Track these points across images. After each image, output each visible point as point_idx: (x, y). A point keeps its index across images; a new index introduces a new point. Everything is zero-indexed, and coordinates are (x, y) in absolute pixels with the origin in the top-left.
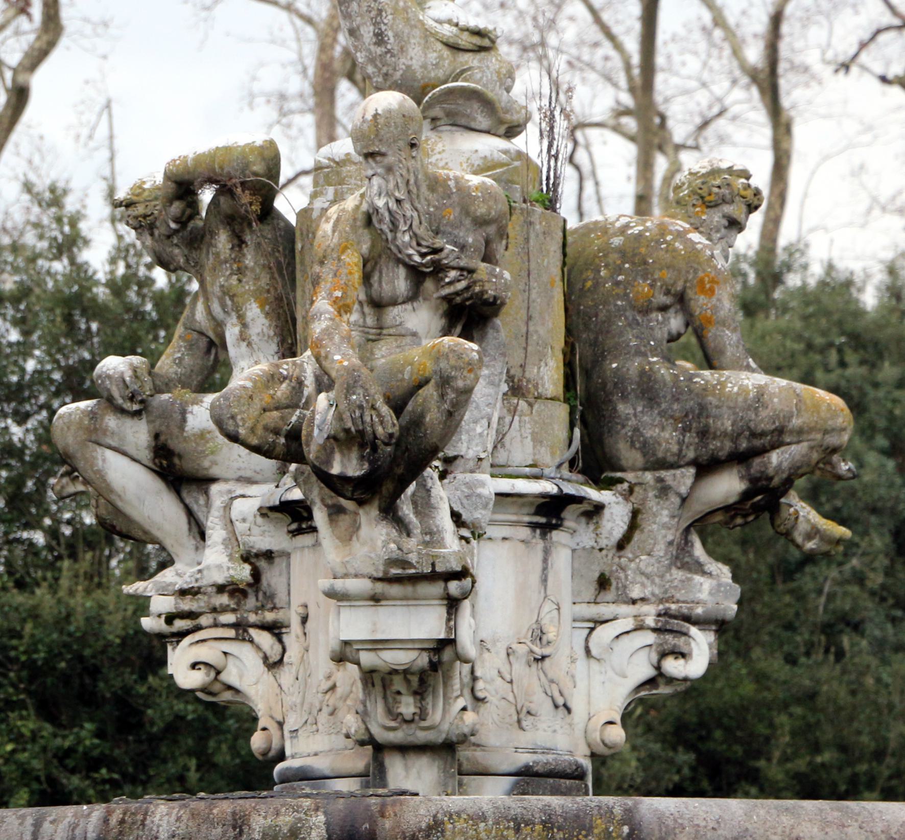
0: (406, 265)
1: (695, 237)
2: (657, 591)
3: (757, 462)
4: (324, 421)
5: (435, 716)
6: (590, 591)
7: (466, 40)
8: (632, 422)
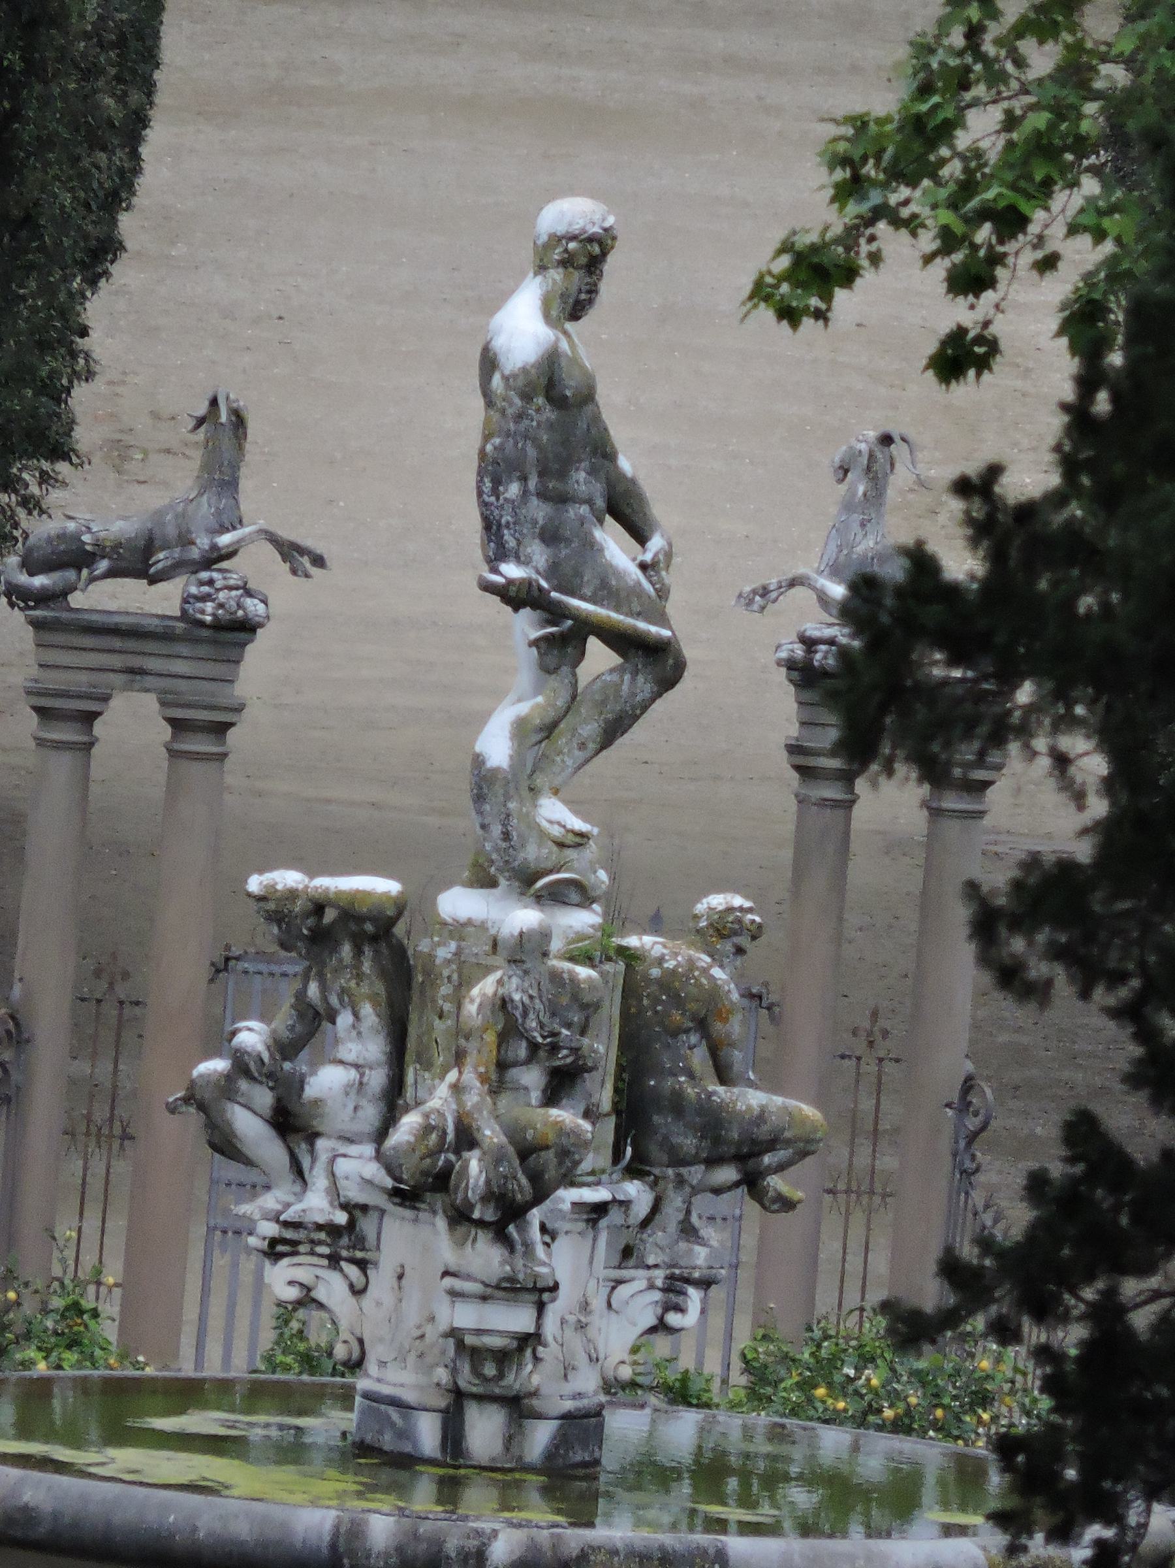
0: (527, 1039)
1: (717, 972)
2: (666, 1260)
3: (751, 1163)
4: (476, 1185)
5: (510, 1378)
6: (616, 1259)
7: (570, 839)
8: (664, 1131)
